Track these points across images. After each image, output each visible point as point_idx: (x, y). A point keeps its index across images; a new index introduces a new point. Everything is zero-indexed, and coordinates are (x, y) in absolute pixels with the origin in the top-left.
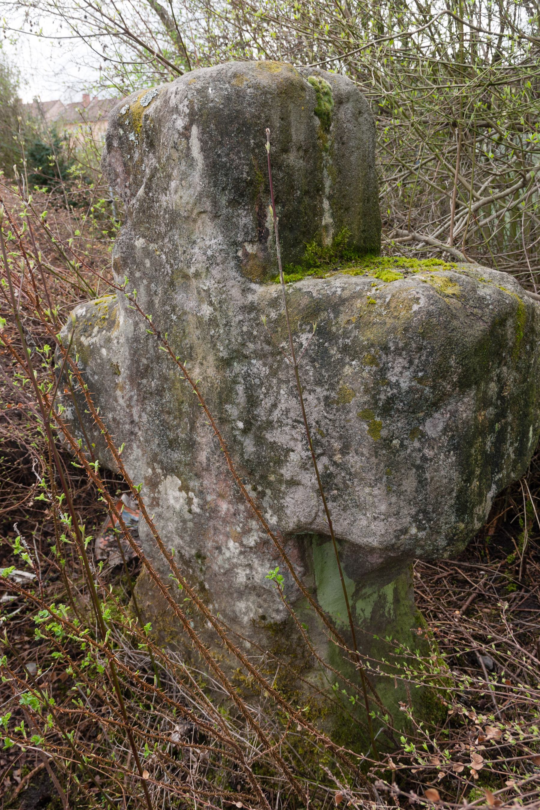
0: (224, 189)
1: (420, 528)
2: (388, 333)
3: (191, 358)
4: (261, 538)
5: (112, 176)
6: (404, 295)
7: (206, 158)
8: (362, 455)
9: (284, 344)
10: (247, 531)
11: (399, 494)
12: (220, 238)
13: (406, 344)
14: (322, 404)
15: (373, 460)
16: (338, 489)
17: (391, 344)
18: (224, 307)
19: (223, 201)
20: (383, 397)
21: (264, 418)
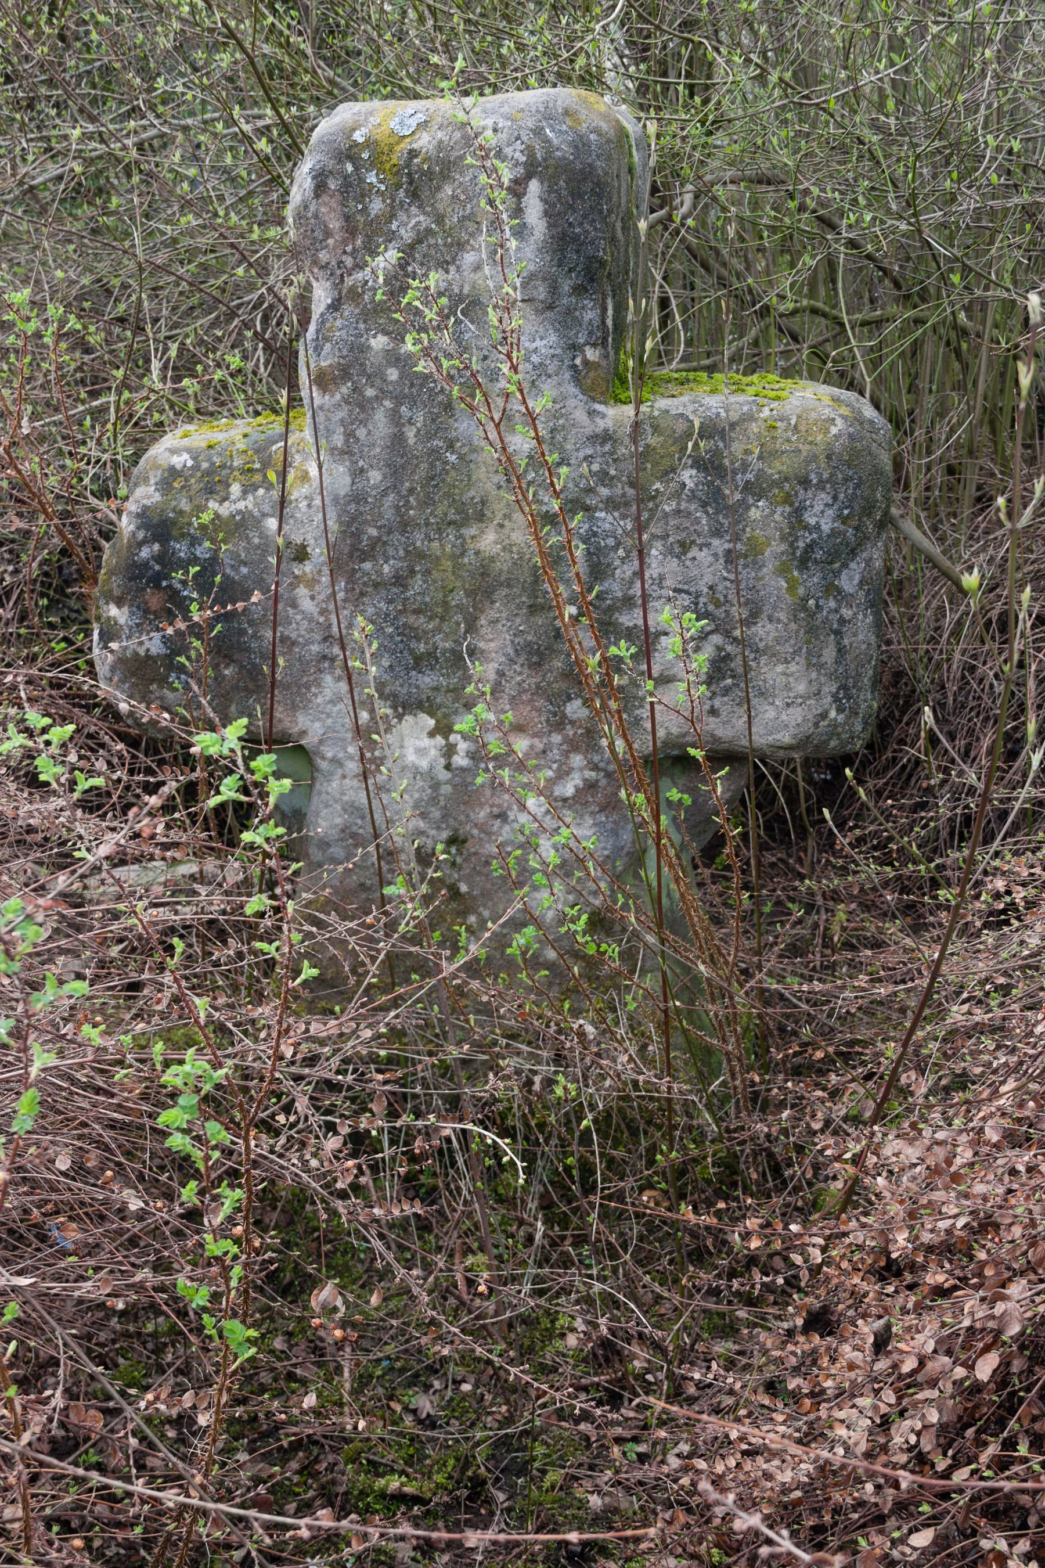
0: (570, 271)
1: (840, 710)
2: (808, 462)
3: (481, 517)
4: (585, 780)
5: (318, 234)
6: (813, 415)
7: (550, 226)
8: (779, 621)
9: (657, 485)
10: (563, 774)
11: (820, 666)
12: (553, 338)
13: (832, 475)
14: (722, 561)
15: (793, 626)
16: (733, 677)
17: (813, 476)
18: (559, 437)
19: (566, 287)
20: (801, 544)
21: (619, 594)
